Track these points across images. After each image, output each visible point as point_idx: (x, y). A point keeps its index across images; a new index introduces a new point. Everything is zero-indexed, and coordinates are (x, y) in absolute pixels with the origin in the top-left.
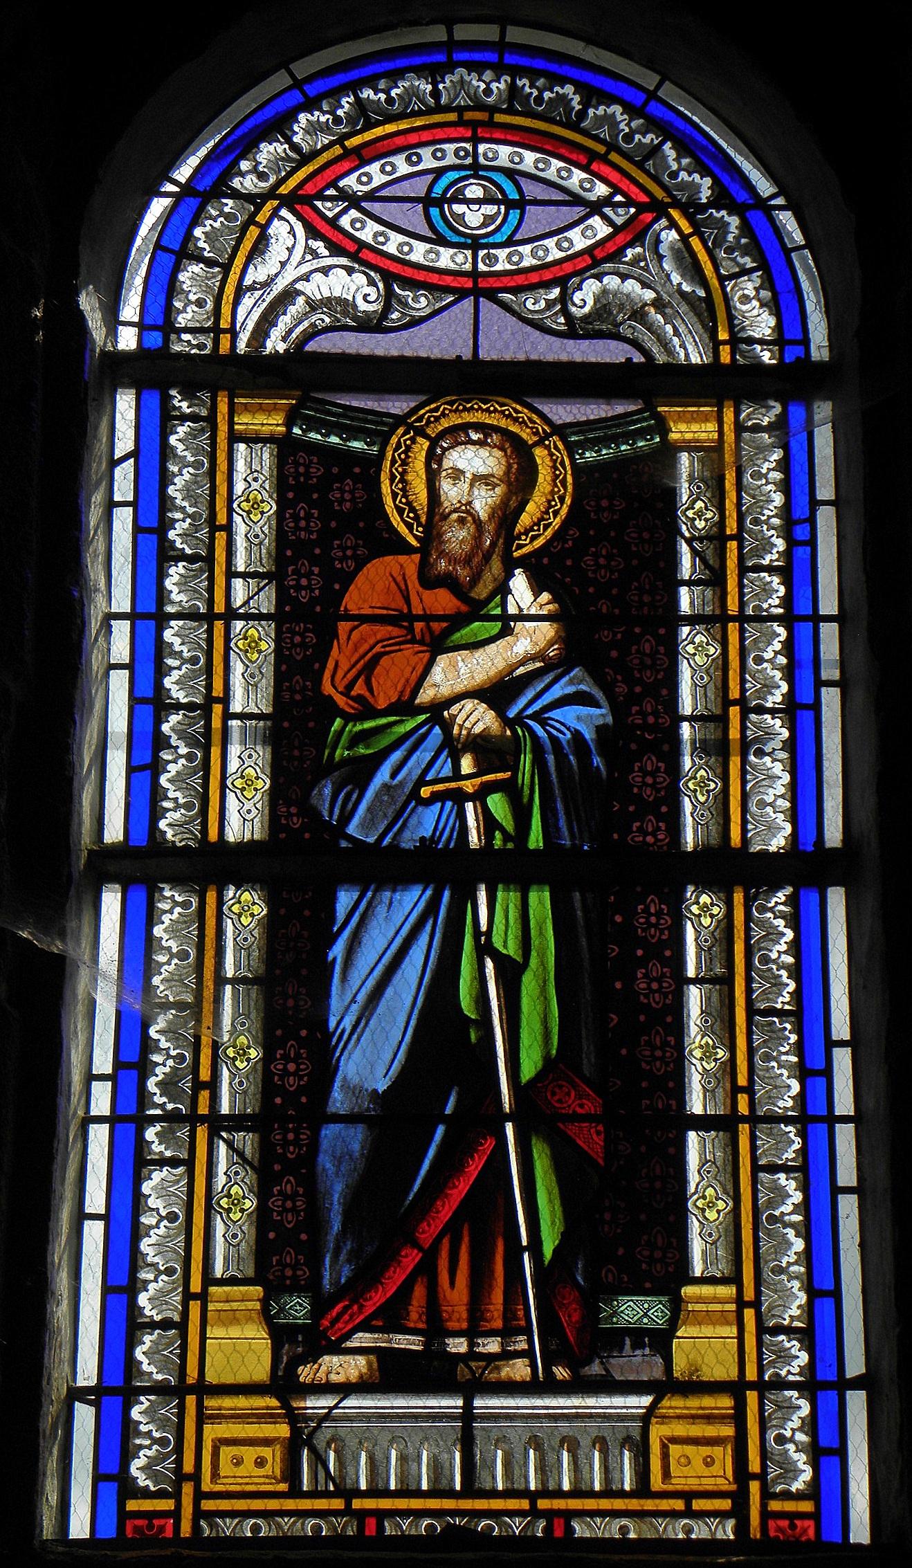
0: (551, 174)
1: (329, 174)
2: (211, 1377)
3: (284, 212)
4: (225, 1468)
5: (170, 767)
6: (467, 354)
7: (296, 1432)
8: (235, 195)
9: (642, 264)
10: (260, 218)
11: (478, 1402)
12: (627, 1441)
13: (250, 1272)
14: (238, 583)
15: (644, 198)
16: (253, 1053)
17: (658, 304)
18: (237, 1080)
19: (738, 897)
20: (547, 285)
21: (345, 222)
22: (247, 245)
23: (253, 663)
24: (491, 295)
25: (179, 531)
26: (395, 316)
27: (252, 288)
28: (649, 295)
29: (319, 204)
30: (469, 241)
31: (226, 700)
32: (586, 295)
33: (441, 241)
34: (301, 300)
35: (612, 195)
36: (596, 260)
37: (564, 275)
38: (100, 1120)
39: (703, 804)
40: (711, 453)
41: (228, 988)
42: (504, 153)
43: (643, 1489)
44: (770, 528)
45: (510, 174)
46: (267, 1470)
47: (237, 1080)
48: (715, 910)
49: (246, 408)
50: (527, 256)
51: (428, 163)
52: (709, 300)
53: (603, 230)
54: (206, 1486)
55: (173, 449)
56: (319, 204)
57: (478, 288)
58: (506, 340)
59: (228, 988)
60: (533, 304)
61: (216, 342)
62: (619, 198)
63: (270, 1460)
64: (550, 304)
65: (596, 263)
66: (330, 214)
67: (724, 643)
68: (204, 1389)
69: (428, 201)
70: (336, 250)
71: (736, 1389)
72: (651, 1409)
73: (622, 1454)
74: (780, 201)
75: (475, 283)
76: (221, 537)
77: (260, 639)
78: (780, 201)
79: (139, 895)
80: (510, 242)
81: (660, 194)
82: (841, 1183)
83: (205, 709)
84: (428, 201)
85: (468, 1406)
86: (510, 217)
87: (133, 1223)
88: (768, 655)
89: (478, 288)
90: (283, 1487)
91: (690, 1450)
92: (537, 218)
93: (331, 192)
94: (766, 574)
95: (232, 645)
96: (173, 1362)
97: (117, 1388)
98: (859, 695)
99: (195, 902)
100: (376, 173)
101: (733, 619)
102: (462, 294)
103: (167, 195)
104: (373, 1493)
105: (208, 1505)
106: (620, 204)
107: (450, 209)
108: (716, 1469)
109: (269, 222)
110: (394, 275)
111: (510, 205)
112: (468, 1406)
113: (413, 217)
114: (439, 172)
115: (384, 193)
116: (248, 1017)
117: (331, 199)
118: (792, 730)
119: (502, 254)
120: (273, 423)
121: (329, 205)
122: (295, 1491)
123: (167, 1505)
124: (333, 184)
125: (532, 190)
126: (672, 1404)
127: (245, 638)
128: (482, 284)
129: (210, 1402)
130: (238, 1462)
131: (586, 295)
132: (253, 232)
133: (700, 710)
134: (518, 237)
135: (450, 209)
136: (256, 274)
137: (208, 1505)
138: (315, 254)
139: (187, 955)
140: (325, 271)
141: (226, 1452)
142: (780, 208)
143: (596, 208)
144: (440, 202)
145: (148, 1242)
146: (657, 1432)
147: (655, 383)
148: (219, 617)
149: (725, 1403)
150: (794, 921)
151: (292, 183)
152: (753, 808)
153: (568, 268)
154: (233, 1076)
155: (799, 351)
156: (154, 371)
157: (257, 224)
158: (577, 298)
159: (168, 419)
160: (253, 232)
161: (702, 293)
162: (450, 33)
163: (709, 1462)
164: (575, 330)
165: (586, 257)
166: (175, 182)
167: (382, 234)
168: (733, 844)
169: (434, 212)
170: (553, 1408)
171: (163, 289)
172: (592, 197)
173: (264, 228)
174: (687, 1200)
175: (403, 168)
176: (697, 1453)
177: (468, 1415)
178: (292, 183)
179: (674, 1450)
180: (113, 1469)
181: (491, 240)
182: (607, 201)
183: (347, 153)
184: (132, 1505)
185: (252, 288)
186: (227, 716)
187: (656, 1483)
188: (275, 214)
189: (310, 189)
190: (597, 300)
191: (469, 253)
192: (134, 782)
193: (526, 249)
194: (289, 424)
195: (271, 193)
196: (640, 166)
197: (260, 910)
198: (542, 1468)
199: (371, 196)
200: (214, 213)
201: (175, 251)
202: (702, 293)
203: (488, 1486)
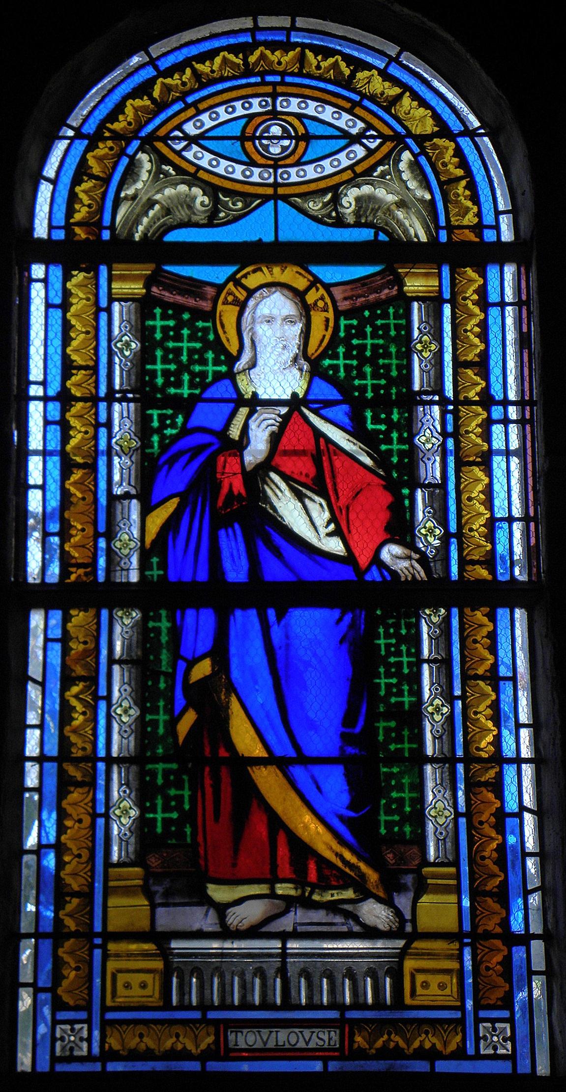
1: (175, 121)
2: (110, 928)
6: (269, 238)
7: (168, 965)
11: (289, 945)
12: (388, 972)
15: (387, 131)
20: (323, 192)
21: (189, 155)
22: (121, 169)
24: (285, 198)
26: (222, 215)
27: (126, 198)
30: (272, 163)
33: (253, 163)
34: (157, 207)
35: (366, 130)
36: (357, 174)
37: (334, 191)
40: (434, 302)
45: (300, 117)
46: (148, 991)
49: (123, 278)
50: (311, 172)
51: (240, 112)
52: (433, 202)
57: (276, 194)
58: (297, 229)
60: (314, 206)
68: (109, 936)
75: (276, 191)
81: (399, 129)
85: (284, 948)
89: (276, 194)
91: (429, 977)
92: (317, 148)
93: (177, 133)
102: (266, 199)
104: (223, 1006)
105: (110, 1016)
106: (372, 137)
111: (298, 138)
112: (284, 948)
115: (210, 134)
116: (129, 685)
117: (179, 139)
119: (293, 171)
120: (137, 288)
124: (179, 127)
125: (315, 129)
128: (281, 191)
129: (112, 947)
132: (125, 161)
134: (304, 160)
137: (110, 1016)
141: (121, 978)
144: (253, 138)
146: (409, 964)
147: (394, 253)
153: (336, 180)
158: (344, 201)
160: (125, 161)
161: (428, 197)
162: (255, 21)
163: (442, 986)
165: (349, 172)
167: (248, 177)
168: (30, 580)
169: (248, 145)
170: (148, 1055)
174: (425, 810)
175: (224, 117)
176: (434, 980)
178: (150, 128)
179: (420, 978)
181: (288, 161)
187: (408, 1000)
189: (162, 132)
194: (147, 286)
196: (387, 110)
198: (332, 991)
199: (202, 136)
202: (428, 197)
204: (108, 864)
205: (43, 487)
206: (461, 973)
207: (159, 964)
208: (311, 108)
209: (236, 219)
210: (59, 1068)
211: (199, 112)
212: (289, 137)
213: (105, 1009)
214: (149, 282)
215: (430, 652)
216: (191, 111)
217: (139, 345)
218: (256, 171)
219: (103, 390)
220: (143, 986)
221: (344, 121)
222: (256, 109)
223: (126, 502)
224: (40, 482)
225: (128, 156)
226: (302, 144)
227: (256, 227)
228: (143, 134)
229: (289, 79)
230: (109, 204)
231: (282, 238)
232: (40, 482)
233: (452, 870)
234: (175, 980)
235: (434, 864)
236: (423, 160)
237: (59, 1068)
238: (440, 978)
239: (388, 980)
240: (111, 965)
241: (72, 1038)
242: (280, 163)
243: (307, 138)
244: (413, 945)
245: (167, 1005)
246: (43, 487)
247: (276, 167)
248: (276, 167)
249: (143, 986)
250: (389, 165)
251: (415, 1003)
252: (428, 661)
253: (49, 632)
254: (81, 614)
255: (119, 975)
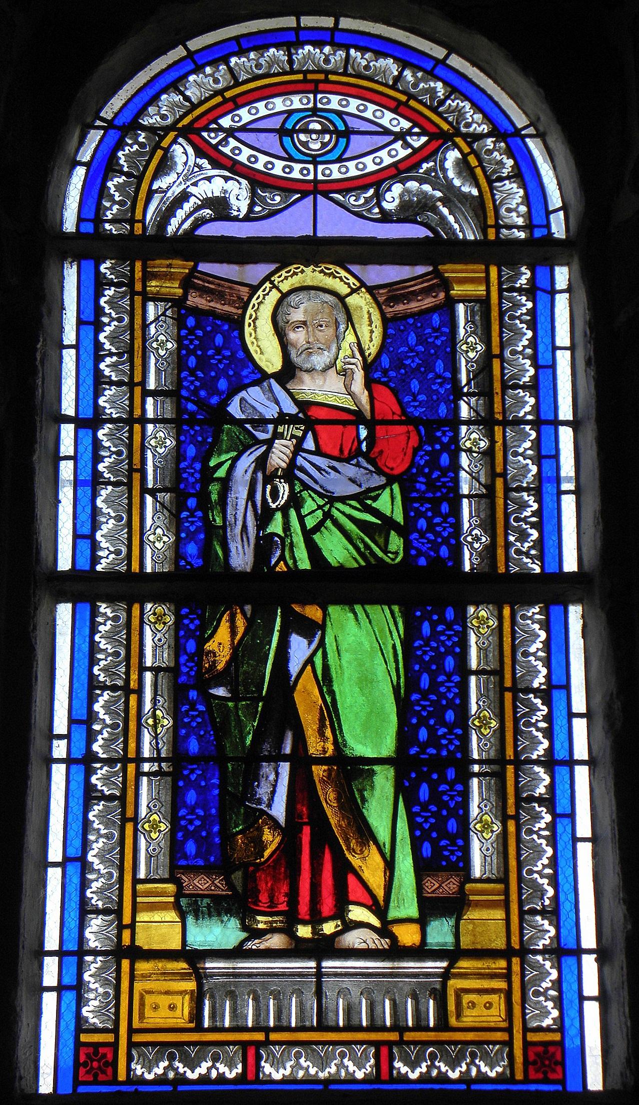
0: (368, 115)
1: (210, 116)
3: (180, 140)
4: (148, 1012)
5: (106, 460)
7: (200, 985)
8: (144, 128)
9: (433, 174)
10: (164, 144)
13: (167, 876)
14: (150, 401)
15: (433, 129)
16: (163, 827)
17: (445, 201)
18: (151, 848)
19: (507, 611)
20: (365, 188)
23: (159, 631)
24: (326, 195)
25: (106, 464)
26: (257, 209)
27: (156, 191)
28: (439, 194)
29: (205, 134)
31: (143, 383)
32: (393, 198)
34: (193, 200)
35: (412, 128)
37: (378, 181)
38: (55, 865)
39: (486, 813)
41: (145, 779)
42: (335, 101)
43: (443, 1024)
44: (540, 837)
45: (340, 114)
47: (151, 848)
48: (491, 623)
53: (403, 153)
54: (136, 1024)
55: (86, 1020)
56: (205, 134)
58: (335, 223)
59: (145, 779)
61: (132, 227)
62: (416, 130)
63: (179, 1006)
64: (367, 201)
65: (400, 172)
66: (214, 142)
67: (500, 618)
69: (283, 132)
70: (215, 164)
71: (507, 953)
72: (447, 969)
73: (291, 999)
74: (531, 130)
76: (133, 699)
77: (165, 614)
78: (531, 130)
79: (85, 609)
80: (340, 160)
82: (579, 835)
83: (130, 421)
84: (283, 132)
85: (319, 967)
86: (339, 144)
87: (95, 273)
88: (532, 649)
90: (192, 1025)
91: (473, 997)
94: (520, 391)
95: (139, 827)
96: (112, 941)
97: (75, 953)
98: (600, 722)
99: (123, 615)
100: (245, 115)
101: (510, 762)
102: (305, 195)
103: (98, 128)
105: (137, 1038)
107: (298, 137)
108: (494, 1011)
109: (170, 145)
110: (259, 182)
111: (340, 134)
112: (319, 967)
113: (271, 142)
114: (290, 113)
117: (213, 130)
118: (558, 928)
119: (335, 167)
121: (213, 135)
122: (199, 1028)
123: (110, 1038)
125: (354, 123)
126: (464, 964)
127: (154, 614)
130: (156, 1008)
131: (393, 198)
132: (160, 153)
133: (484, 756)
134: (345, 156)
135: (298, 137)
136: (162, 183)
137: (137, 1038)
138: (200, 168)
139: (122, 519)
140: (209, 179)
142: (530, 136)
143: (401, 136)
144: (291, 133)
145: (93, 840)
147: (439, 250)
148: (131, 760)
149: (503, 963)
150: (547, 626)
151: (186, 121)
152: (519, 657)
154: (149, 844)
155: (544, 231)
156: (89, 246)
157: (162, 148)
159: (100, 284)
160: (160, 153)
161: (475, 192)
164: (386, 217)
165: (393, 169)
166: (103, 120)
169: (287, 140)
171: (95, 191)
172: (397, 129)
173: (167, 150)
174: (469, 824)
175: (263, 112)
177: (319, 974)
178: (186, 121)
180: (86, 530)
182: (409, 132)
183: (225, 101)
184: (84, 1038)
185: (156, 191)
186: (139, 774)
187: (453, 1021)
188: (174, 141)
190: (401, 196)
191: (311, 96)
192: (82, 333)
193: (351, 165)
195: (172, 127)
197: (170, 443)
199: (244, 129)
200: (130, 142)
201: (104, 167)
202: (475, 192)
203: (332, 1023)
204: (136, 881)
205: (75, 458)
206: (508, 994)
207: (191, 985)
208: (353, 105)
209: (273, 214)
210: (82, 1089)
211: (238, 107)
212: (330, 132)
213: (131, 1031)
214: (187, 283)
215: (479, 664)
216: (230, 105)
217: (175, 346)
218: (297, 167)
219: (132, 754)
220: (172, 1008)
221: (387, 119)
222: (297, 105)
223: (158, 486)
224: (71, 452)
225: (162, 148)
226: (343, 141)
227: (294, 223)
228: (180, 125)
229: (332, 78)
230: (142, 195)
231: (320, 234)
232: (71, 452)
233: (500, 887)
234: (207, 1002)
235: (480, 881)
236: (472, 160)
237: (82, 1089)
238: (486, 998)
239: (431, 1002)
240: (138, 986)
241: (95, 1064)
242: (318, 159)
243: (348, 133)
244: (458, 965)
245: (199, 1028)
246: (75, 458)
247: (316, 163)
248: (316, 163)
249: (172, 1008)
250: (435, 162)
251: (461, 1025)
252: (477, 673)
253: (74, 713)
254: (106, 768)
255: (147, 997)
